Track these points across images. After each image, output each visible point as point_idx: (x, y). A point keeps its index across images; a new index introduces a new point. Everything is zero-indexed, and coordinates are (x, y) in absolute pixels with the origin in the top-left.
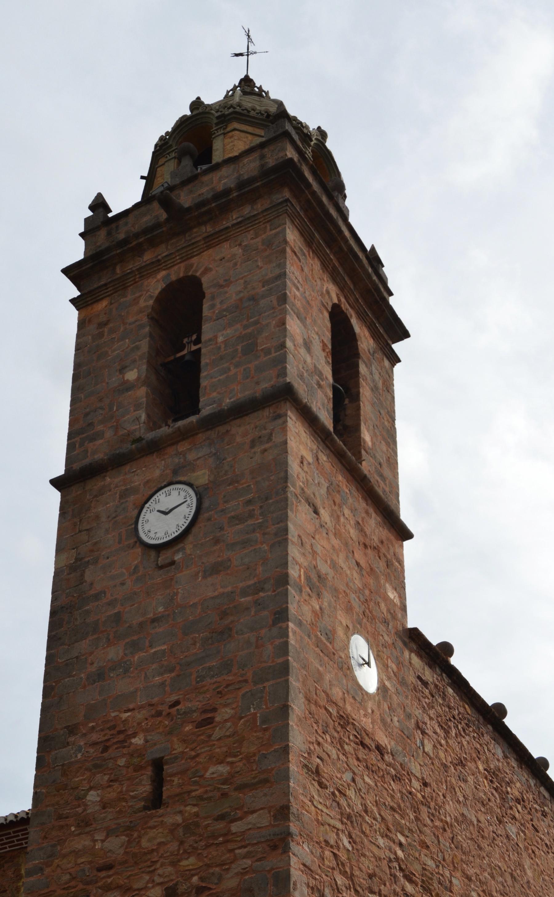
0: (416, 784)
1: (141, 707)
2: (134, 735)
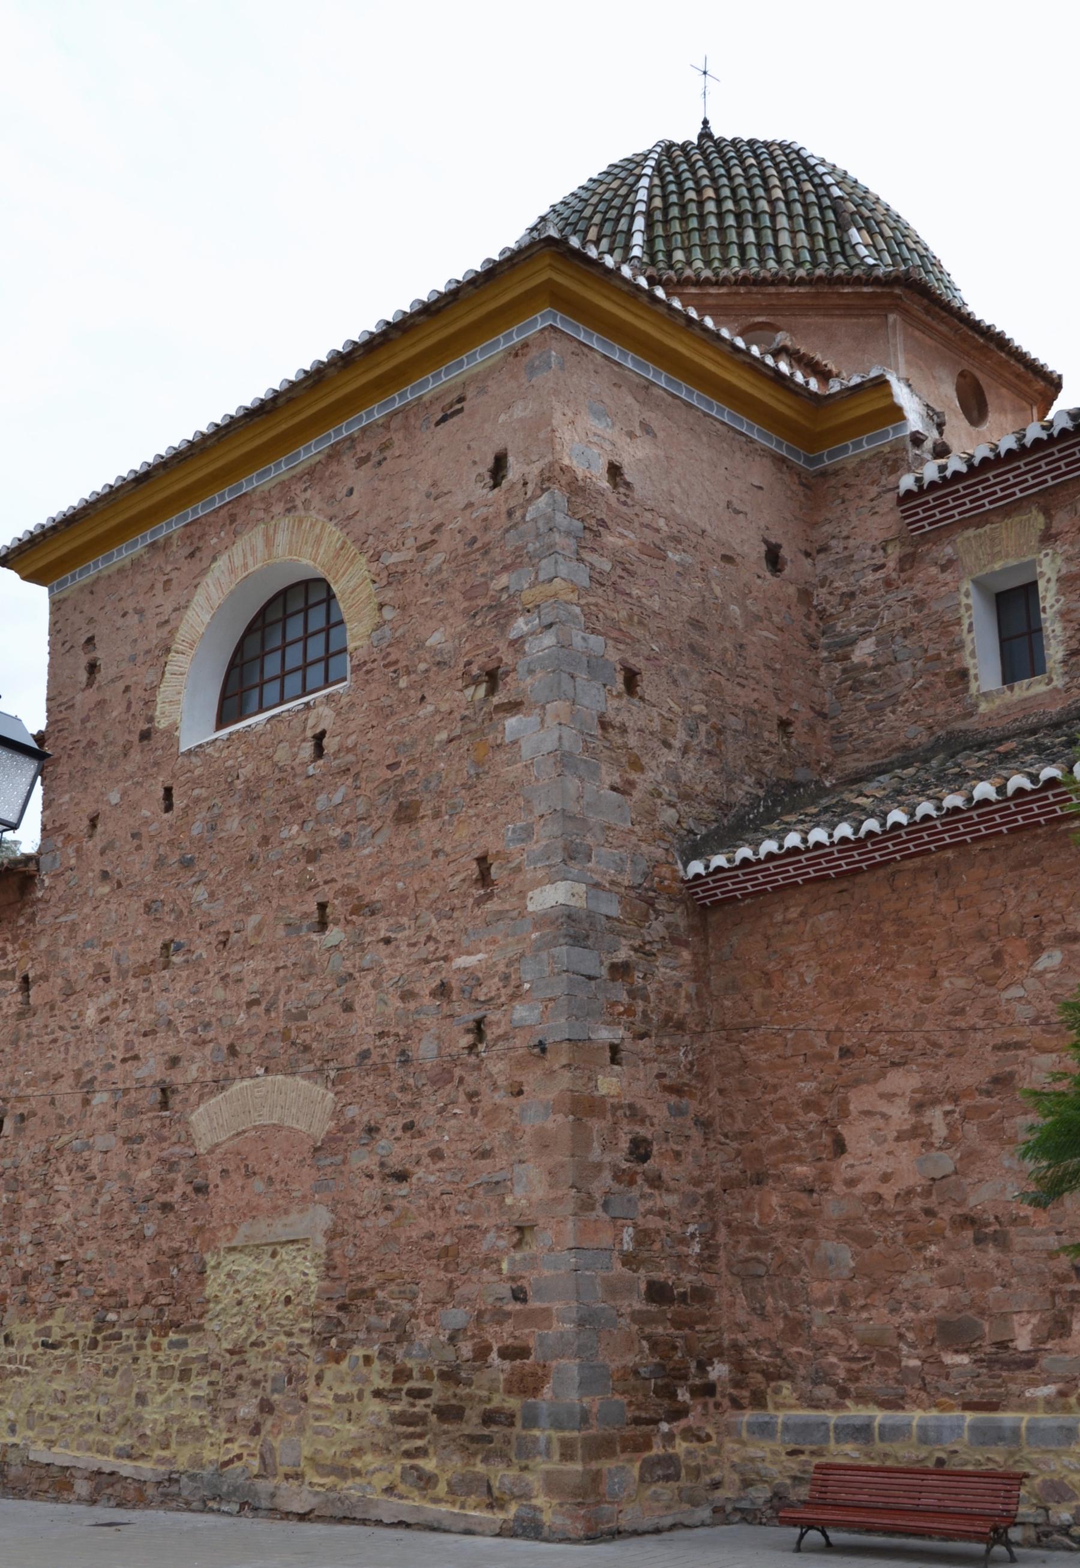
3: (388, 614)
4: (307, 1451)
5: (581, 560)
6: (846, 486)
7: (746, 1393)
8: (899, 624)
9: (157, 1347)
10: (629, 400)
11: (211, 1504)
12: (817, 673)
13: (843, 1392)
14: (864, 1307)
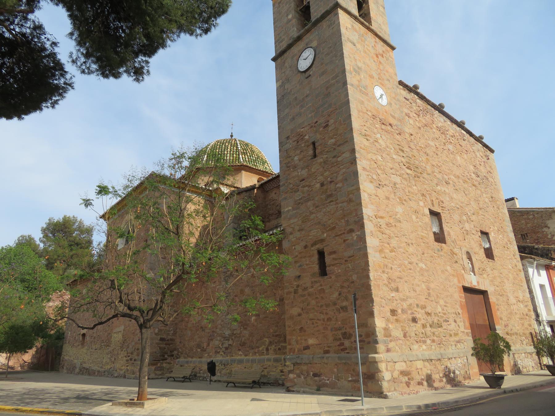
0: (407, 136)
1: (306, 126)
2: (305, 135)
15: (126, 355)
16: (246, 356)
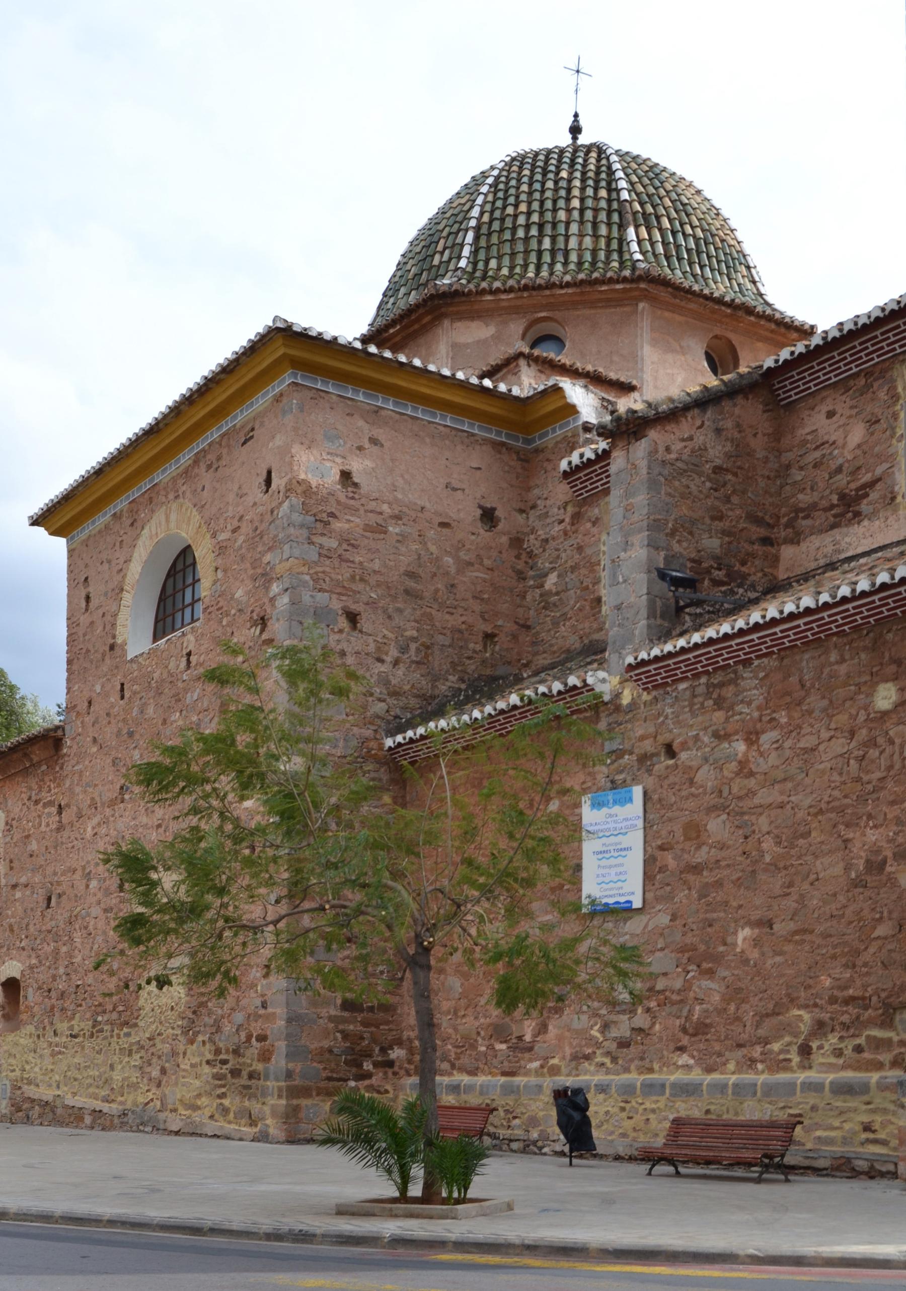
3: (220, 574)
4: (179, 1096)
5: (311, 543)
6: (548, 460)
7: (412, 1067)
8: (570, 563)
9: (119, 1037)
10: (361, 423)
11: (141, 1128)
12: (524, 597)
13: (453, 1066)
14: (464, 1016)
15: (209, 1057)
16: (709, 1070)
